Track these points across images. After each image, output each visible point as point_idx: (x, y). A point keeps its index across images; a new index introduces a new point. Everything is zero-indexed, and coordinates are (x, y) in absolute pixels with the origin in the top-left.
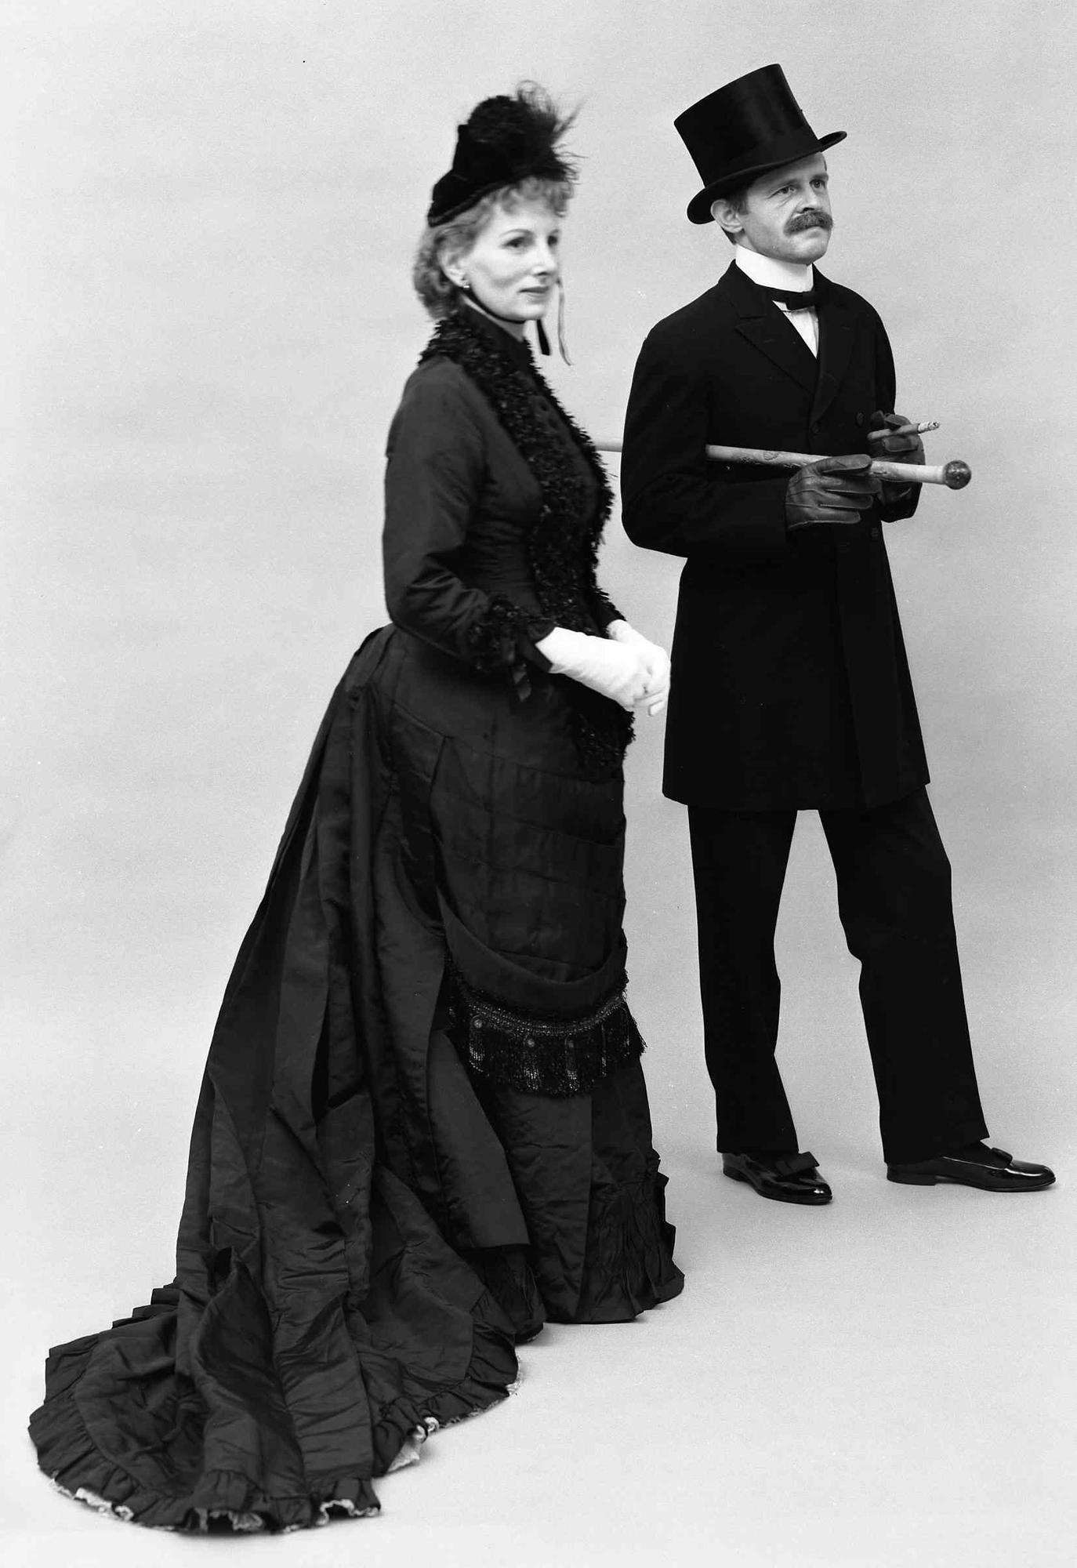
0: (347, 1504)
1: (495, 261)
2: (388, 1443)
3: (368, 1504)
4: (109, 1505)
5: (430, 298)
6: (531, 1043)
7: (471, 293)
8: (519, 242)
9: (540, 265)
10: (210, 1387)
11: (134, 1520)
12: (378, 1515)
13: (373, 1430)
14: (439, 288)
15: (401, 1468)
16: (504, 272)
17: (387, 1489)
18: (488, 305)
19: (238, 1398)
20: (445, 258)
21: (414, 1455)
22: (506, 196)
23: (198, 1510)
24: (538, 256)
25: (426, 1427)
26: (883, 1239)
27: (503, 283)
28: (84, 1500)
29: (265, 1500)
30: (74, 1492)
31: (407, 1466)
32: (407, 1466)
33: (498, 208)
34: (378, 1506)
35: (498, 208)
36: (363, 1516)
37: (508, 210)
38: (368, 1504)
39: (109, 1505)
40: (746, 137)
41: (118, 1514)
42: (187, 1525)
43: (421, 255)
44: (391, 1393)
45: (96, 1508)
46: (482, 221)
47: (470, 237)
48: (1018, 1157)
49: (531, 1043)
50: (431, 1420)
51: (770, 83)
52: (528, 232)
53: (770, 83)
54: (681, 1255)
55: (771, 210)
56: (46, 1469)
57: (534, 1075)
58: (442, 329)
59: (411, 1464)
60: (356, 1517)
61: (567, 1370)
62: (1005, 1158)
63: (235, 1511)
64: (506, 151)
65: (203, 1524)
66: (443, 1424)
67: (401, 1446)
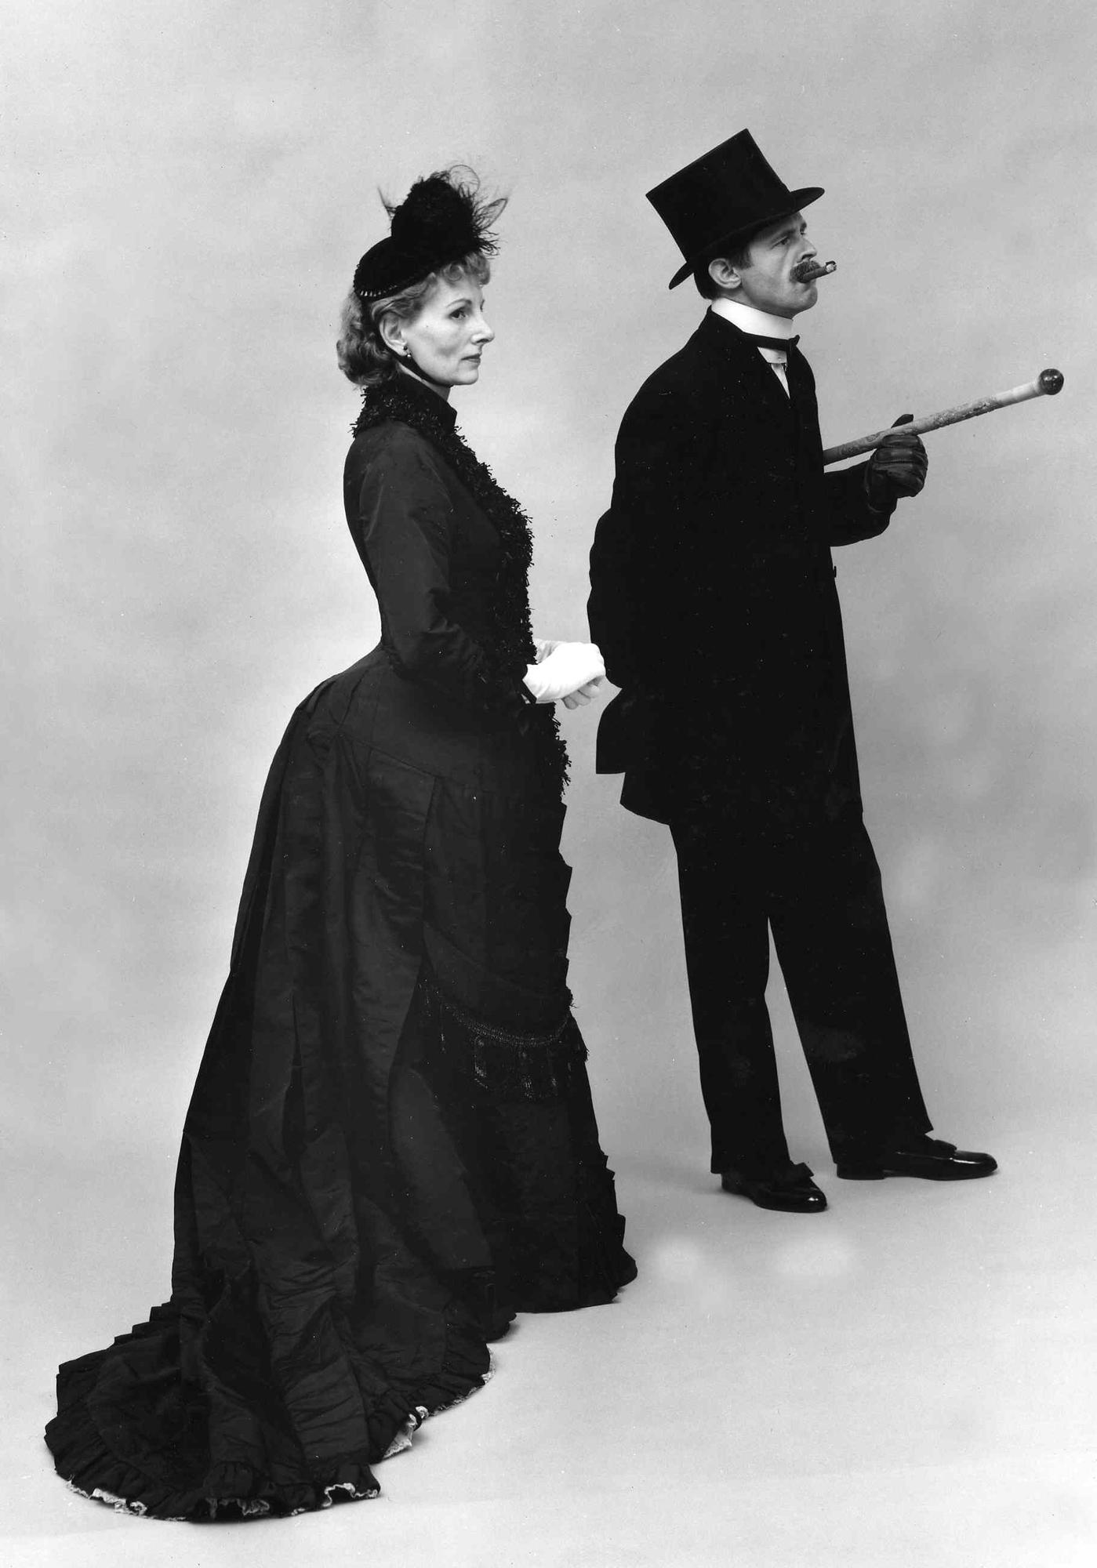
0: (349, 1486)
1: (428, 334)
2: (383, 1429)
3: (368, 1487)
4: (124, 1501)
5: (357, 366)
6: (481, 1043)
7: (411, 363)
8: (458, 314)
9: (480, 332)
10: (213, 1386)
11: (148, 1514)
12: (378, 1496)
13: (367, 1420)
14: (377, 355)
15: (395, 1455)
16: (446, 342)
17: (383, 1472)
18: (431, 373)
19: (231, 1392)
20: (385, 331)
21: (406, 1442)
22: (453, 270)
23: (210, 1501)
24: (477, 325)
25: (417, 1415)
26: (866, 1231)
27: (447, 352)
28: (100, 1499)
29: (271, 1487)
30: (90, 1492)
31: (401, 1452)
32: (401, 1452)
33: (442, 284)
34: (378, 1488)
35: (442, 284)
36: (364, 1498)
37: (452, 284)
38: (368, 1487)
39: (124, 1501)
40: (725, 205)
41: (132, 1509)
42: (198, 1515)
43: (352, 326)
44: (382, 1386)
45: (112, 1505)
46: (428, 294)
47: (411, 311)
48: (962, 1147)
49: (481, 1043)
50: (420, 1409)
51: (740, 153)
52: (469, 302)
53: (740, 153)
54: (631, 1243)
55: (769, 263)
56: (63, 1471)
57: (528, 1085)
58: (371, 398)
59: (406, 1450)
60: (358, 1499)
61: (533, 1353)
62: (948, 1149)
63: (243, 1498)
64: (435, 234)
65: (213, 1512)
66: (431, 1413)
67: (395, 1435)
